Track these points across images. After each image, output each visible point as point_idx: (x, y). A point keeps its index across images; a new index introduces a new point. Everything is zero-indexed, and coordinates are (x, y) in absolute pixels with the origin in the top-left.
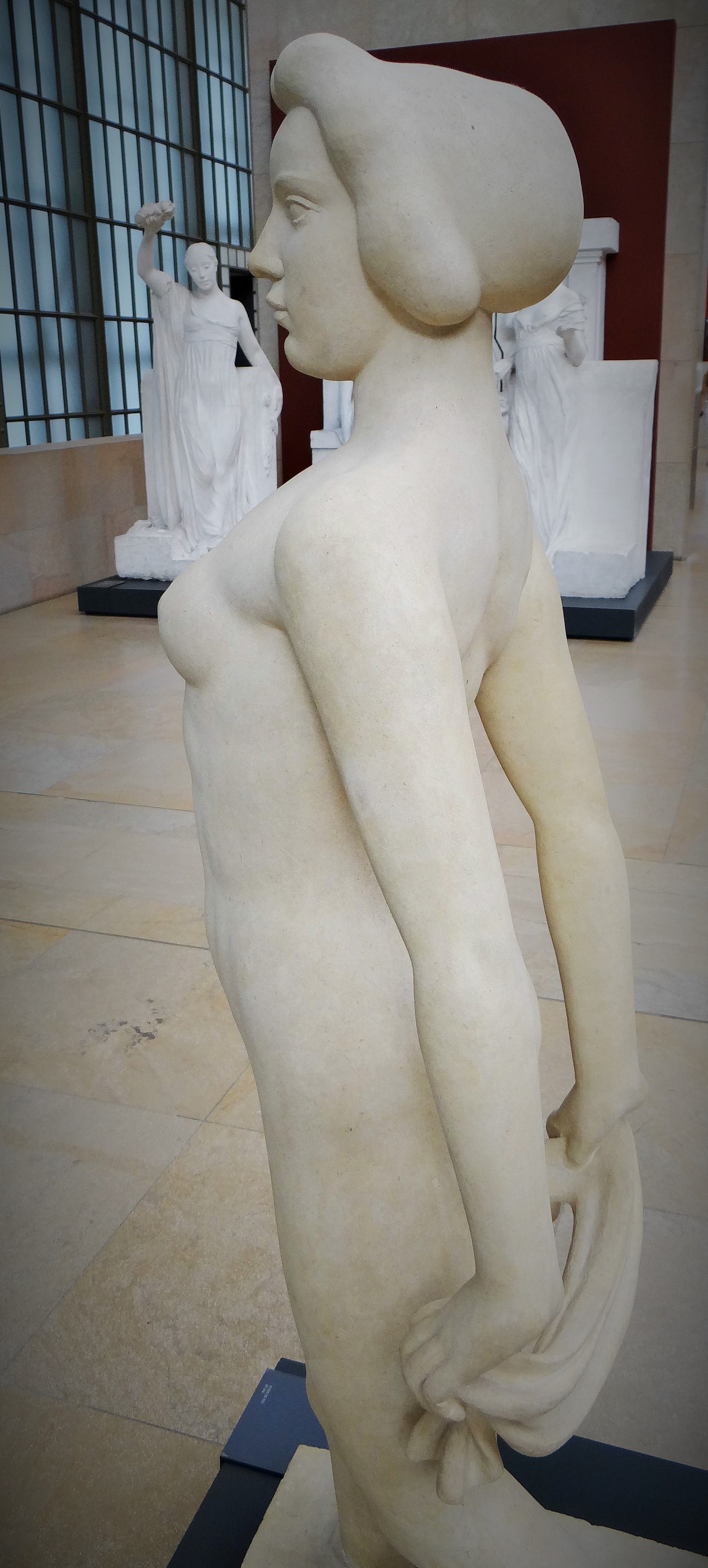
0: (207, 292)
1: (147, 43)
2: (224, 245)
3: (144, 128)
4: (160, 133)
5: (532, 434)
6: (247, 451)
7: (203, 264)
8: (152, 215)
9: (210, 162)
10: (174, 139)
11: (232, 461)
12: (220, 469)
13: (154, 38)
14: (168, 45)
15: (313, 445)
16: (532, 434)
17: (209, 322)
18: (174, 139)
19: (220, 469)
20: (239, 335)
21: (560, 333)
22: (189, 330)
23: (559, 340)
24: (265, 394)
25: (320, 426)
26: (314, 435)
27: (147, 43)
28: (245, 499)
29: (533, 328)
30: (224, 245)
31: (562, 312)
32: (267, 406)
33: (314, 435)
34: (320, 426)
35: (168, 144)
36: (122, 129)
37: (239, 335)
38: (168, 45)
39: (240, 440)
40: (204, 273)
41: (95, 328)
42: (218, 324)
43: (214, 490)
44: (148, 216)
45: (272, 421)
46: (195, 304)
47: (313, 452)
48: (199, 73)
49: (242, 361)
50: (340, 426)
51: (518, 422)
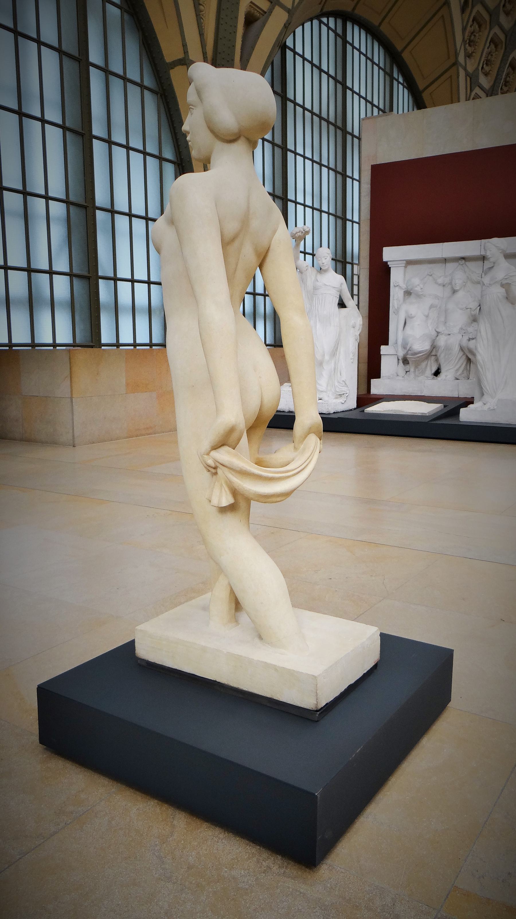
0: (326, 271)
1: (321, 165)
2: (356, 264)
3: (316, 206)
4: (325, 208)
5: (488, 339)
6: (342, 350)
7: (324, 257)
8: (299, 232)
9: (351, 223)
10: (332, 211)
11: (334, 353)
12: (327, 358)
13: (325, 162)
14: (332, 165)
15: (382, 353)
16: (488, 339)
17: (325, 285)
18: (332, 211)
19: (327, 358)
20: (340, 291)
21: (502, 286)
22: (315, 288)
23: (503, 290)
24: (353, 322)
25: (387, 343)
26: (383, 348)
27: (321, 165)
28: (339, 373)
29: (490, 284)
30: (356, 264)
31: (506, 276)
32: (354, 327)
33: (383, 348)
34: (387, 343)
35: (329, 213)
36: (305, 205)
37: (340, 291)
38: (332, 165)
39: (338, 344)
40: (324, 261)
41: (80, 66)
42: (329, 286)
43: (323, 368)
44: (297, 233)
45: (356, 335)
46: (319, 277)
47: (382, 357)
48: (289, 153)
49: (342, 305)
50: (397, 343)
51: (480, 332)
